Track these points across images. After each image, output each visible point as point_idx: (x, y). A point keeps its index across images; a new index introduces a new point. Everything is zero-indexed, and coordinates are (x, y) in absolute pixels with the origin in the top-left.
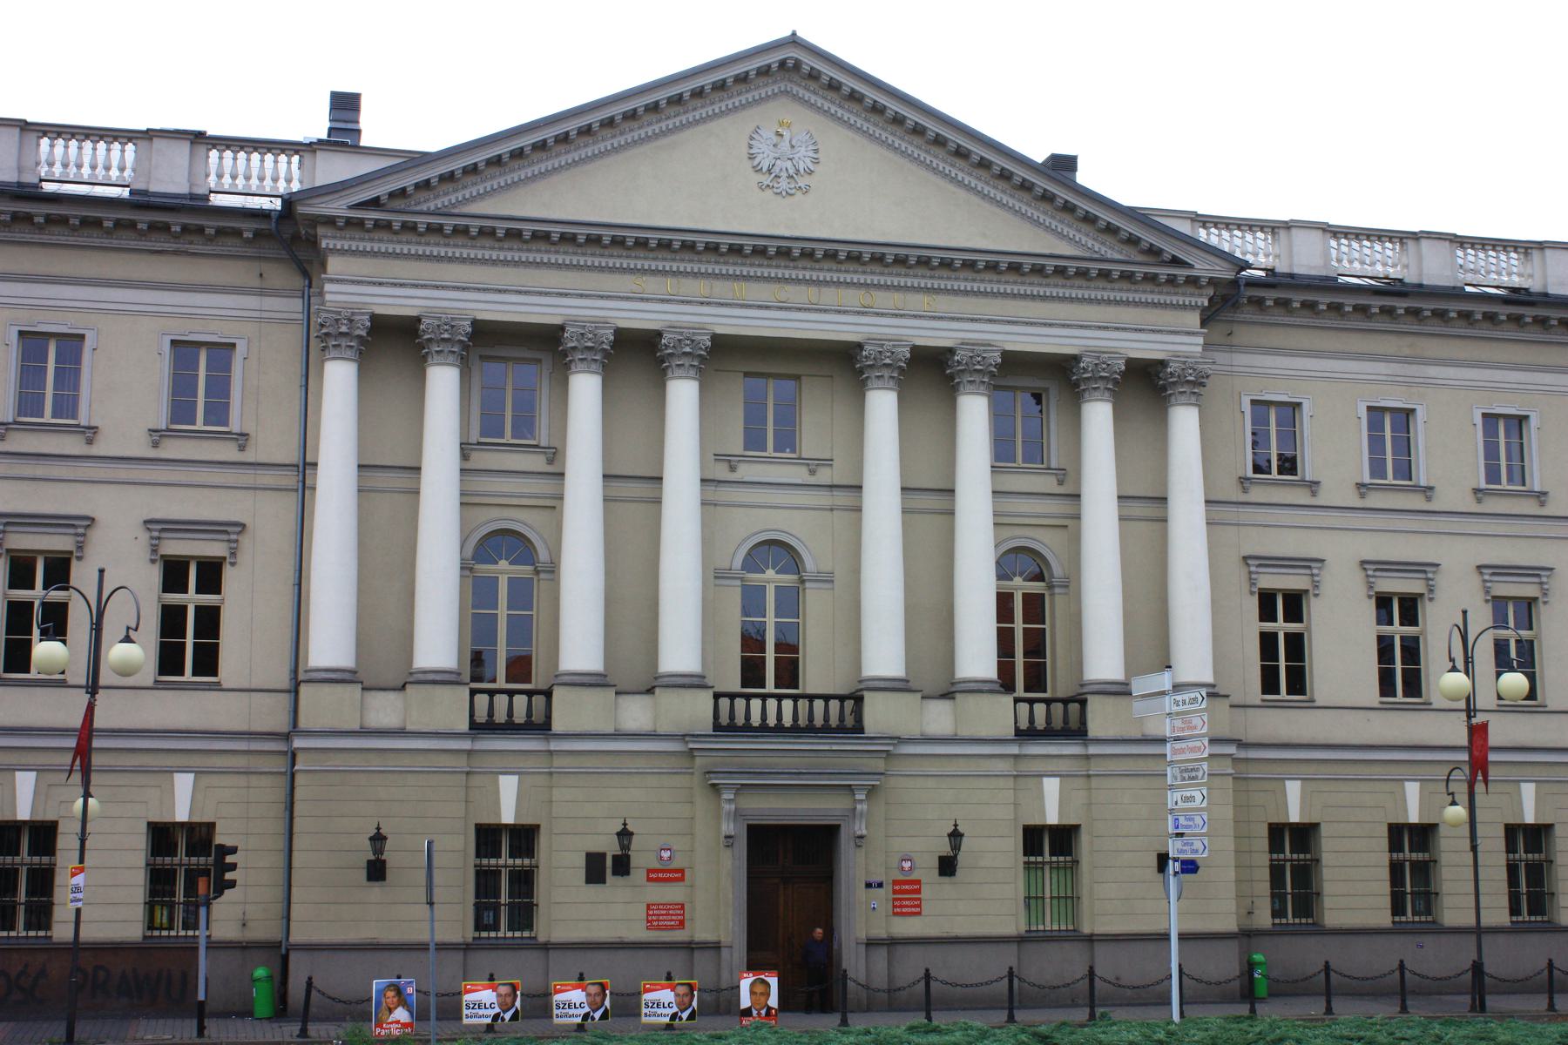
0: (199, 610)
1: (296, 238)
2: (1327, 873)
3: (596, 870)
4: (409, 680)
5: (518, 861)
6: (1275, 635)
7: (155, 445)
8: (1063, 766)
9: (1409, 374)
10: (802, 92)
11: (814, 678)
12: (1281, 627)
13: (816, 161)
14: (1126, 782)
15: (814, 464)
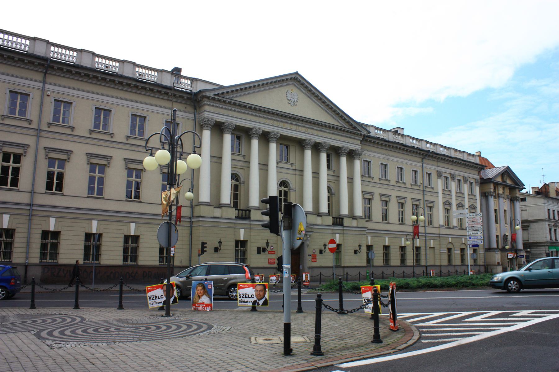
0: (58, 173)
1: (196, 100)
2: (391, 255)
3: (260, 250)
5: (8, 239)
6: (95, 178)
8: (339, 232)
9: (97, 97)
10: (296, 84)
12: (56, 170)
14: (349, 235)
15: (292, 165)
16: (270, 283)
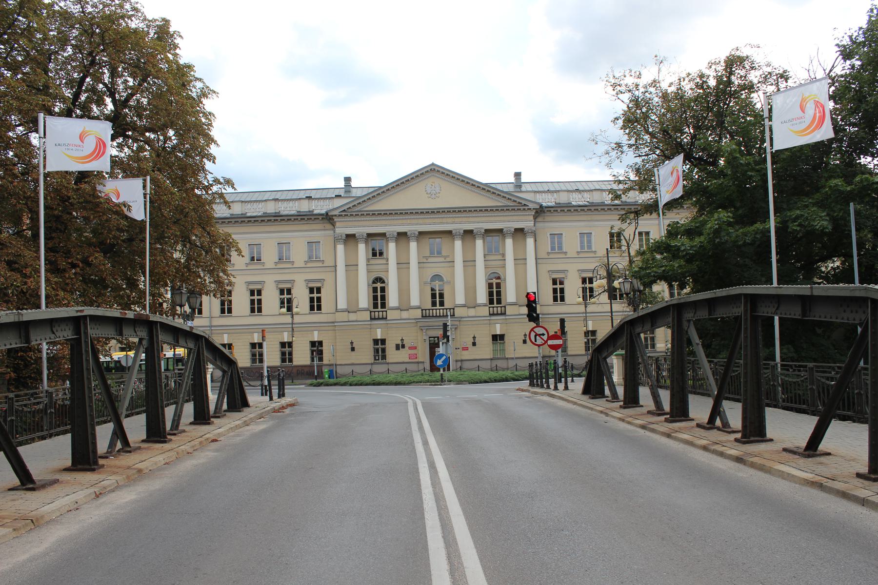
1: (330, 219)
3: (398, 347)
4: (409, 308)
6: (314, 297)
7: (276, 265)
8: (500, 321)
11: (447, 304)
13: (441, 190)
15: (445, 257)
16: (259, 383)
